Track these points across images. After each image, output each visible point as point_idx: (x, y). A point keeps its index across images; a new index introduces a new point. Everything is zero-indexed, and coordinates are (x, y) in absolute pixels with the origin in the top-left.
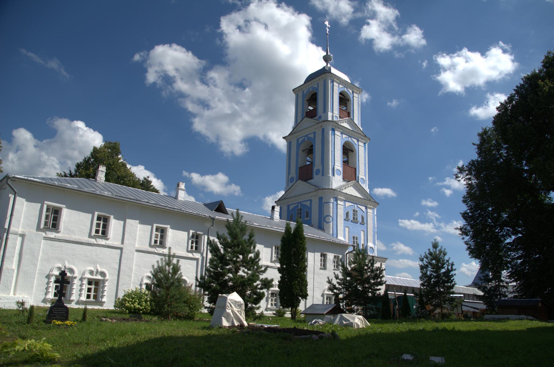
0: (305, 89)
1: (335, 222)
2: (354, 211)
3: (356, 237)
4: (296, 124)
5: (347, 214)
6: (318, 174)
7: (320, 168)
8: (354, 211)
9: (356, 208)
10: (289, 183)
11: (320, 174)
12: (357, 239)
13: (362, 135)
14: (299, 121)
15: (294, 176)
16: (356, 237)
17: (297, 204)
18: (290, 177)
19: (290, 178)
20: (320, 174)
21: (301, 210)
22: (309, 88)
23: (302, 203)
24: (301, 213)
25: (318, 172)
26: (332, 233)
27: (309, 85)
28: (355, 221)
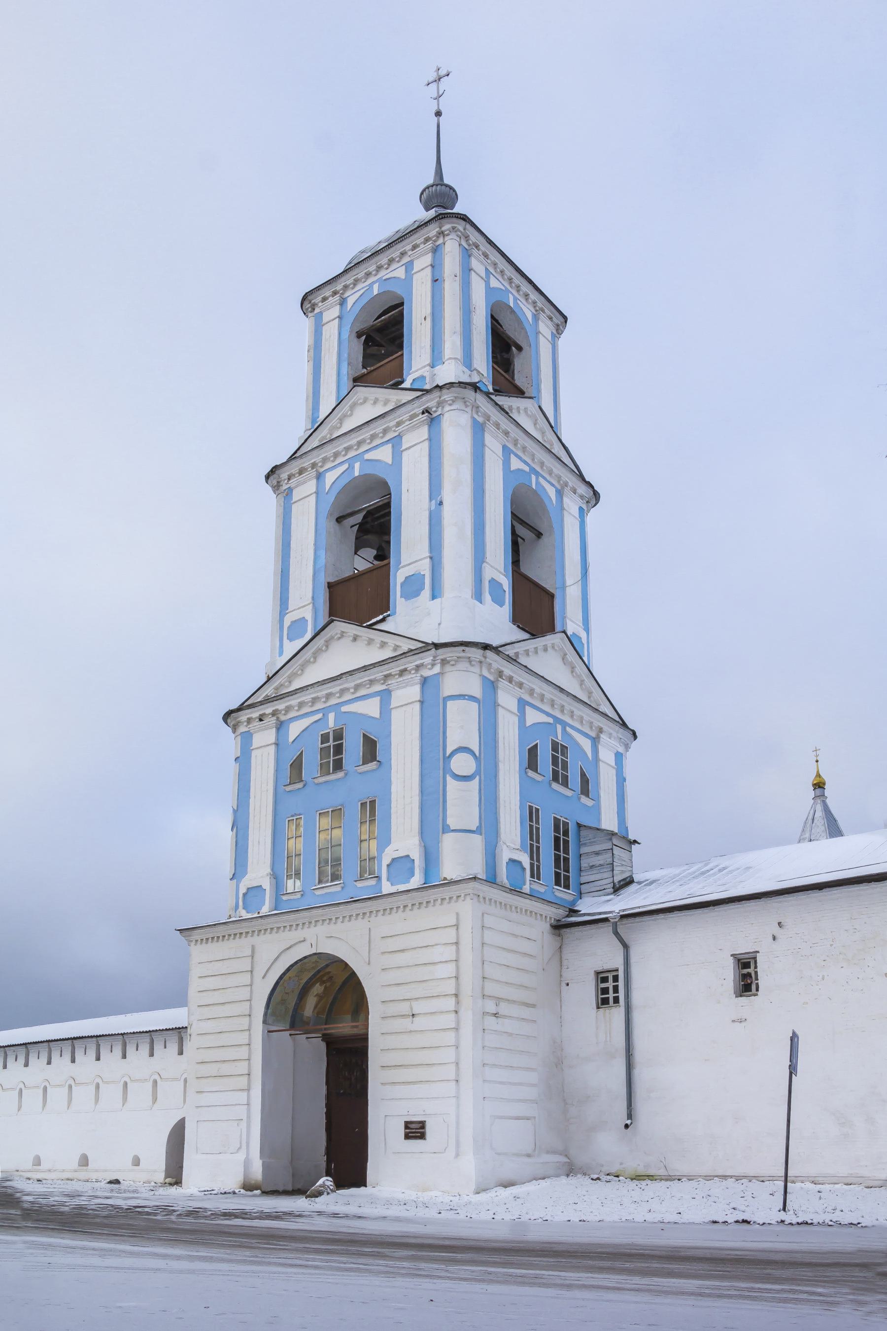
0: (292, 714)
1: (443, 1274)
2: (555, 746)
3: (558, 883)
4: (314, 421)
5: (533, 752)
6: (417, 593)
7: (425, 567)
8: (555, 746)
9: (560, 737)
10: (285, 641)
11: (426, 592)
12: (557, 875)
13: (605, 715)
14: (326, 405)
15: (308, 614)
16: (558, 883)
17: (346, 466)
18: (245, 884)
19: (287, 622)
20: (426, 592)
21: (339, 735)
23: (367, 457)
24: (339, 749)
25: (413, 587)
26: (489, 439)
27: (368, 275)
28: (559, 777)
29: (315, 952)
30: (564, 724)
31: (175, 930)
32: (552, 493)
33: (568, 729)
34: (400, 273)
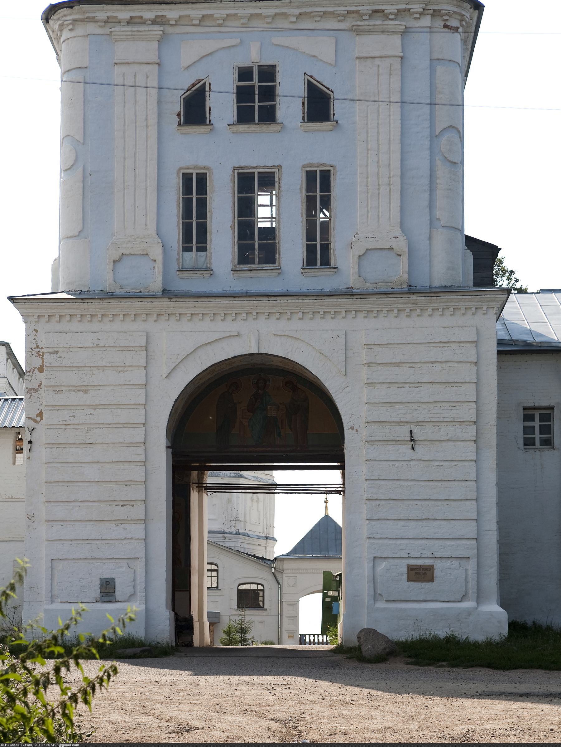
29: (256, 351)
31: (12, 299)
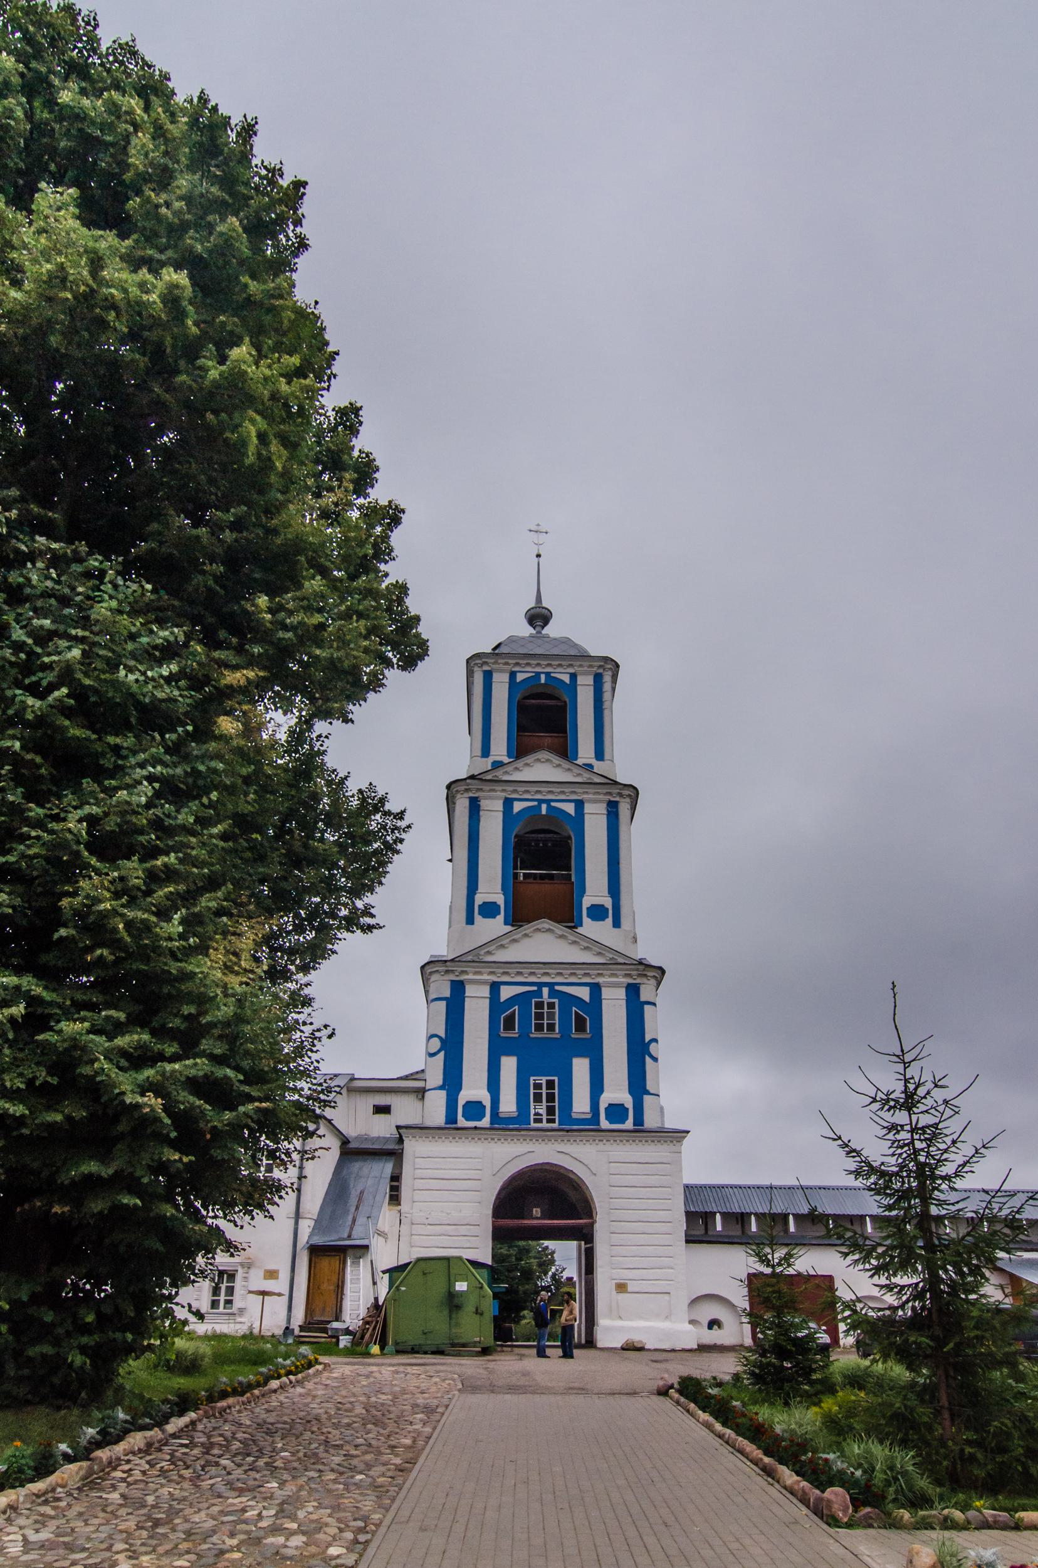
22: (538, 674)
30: (550, 985)
32: (570, 808)
33: (553, 804)
34: (566, 679)
